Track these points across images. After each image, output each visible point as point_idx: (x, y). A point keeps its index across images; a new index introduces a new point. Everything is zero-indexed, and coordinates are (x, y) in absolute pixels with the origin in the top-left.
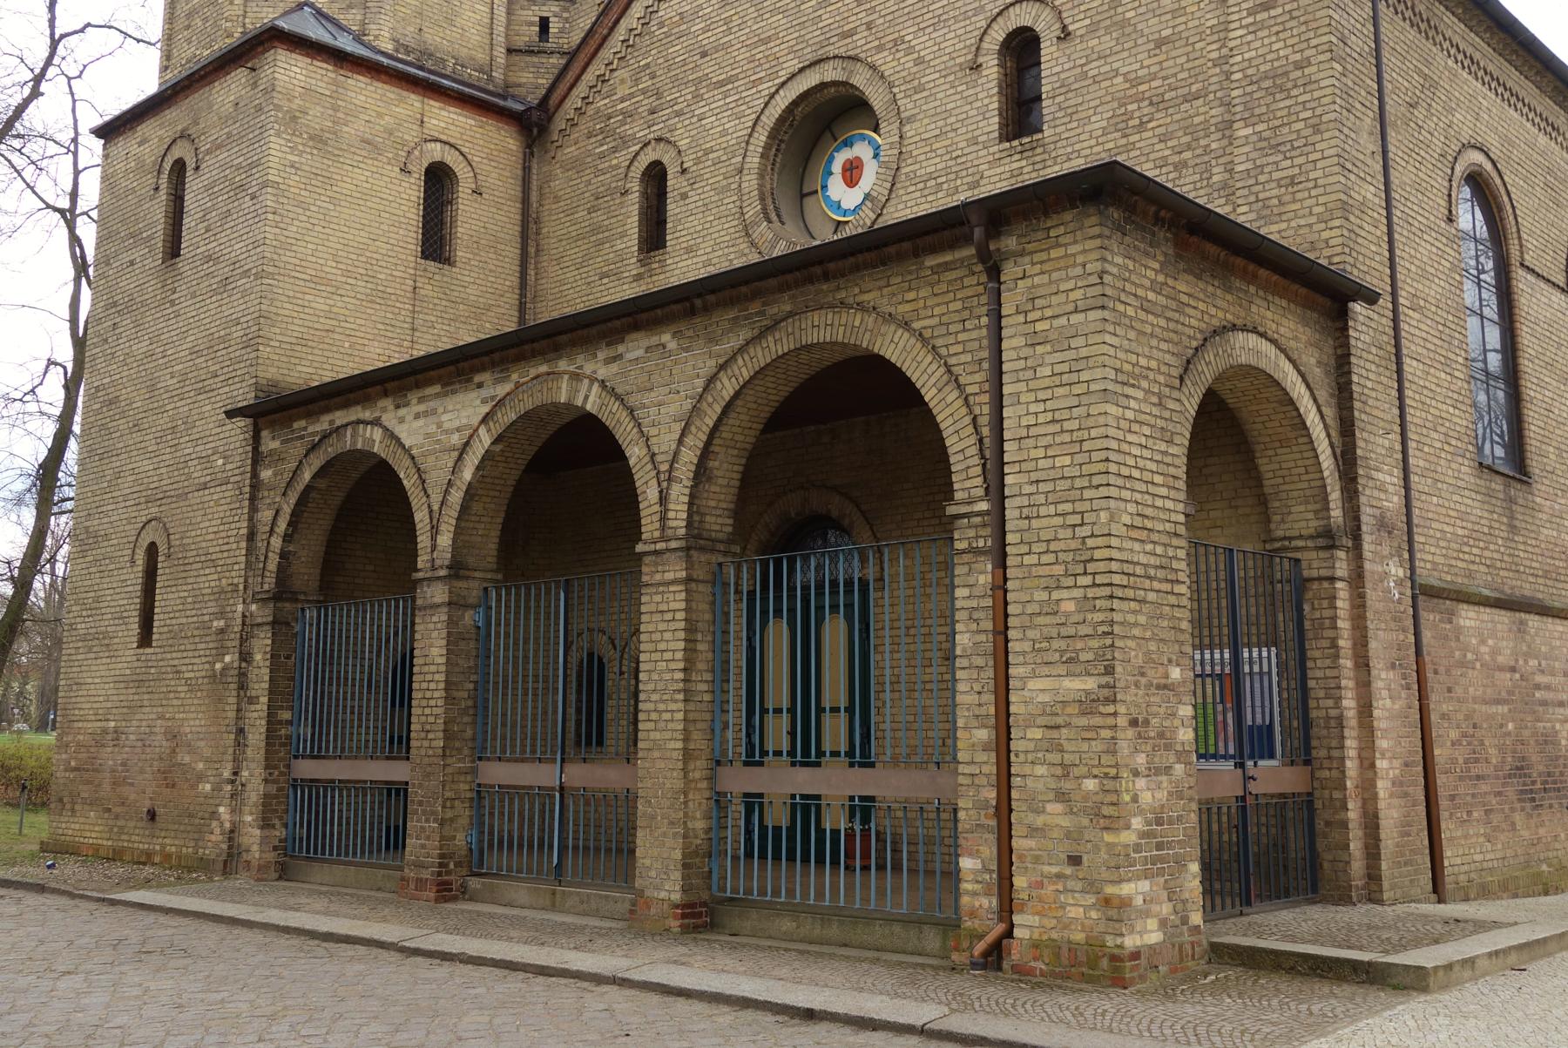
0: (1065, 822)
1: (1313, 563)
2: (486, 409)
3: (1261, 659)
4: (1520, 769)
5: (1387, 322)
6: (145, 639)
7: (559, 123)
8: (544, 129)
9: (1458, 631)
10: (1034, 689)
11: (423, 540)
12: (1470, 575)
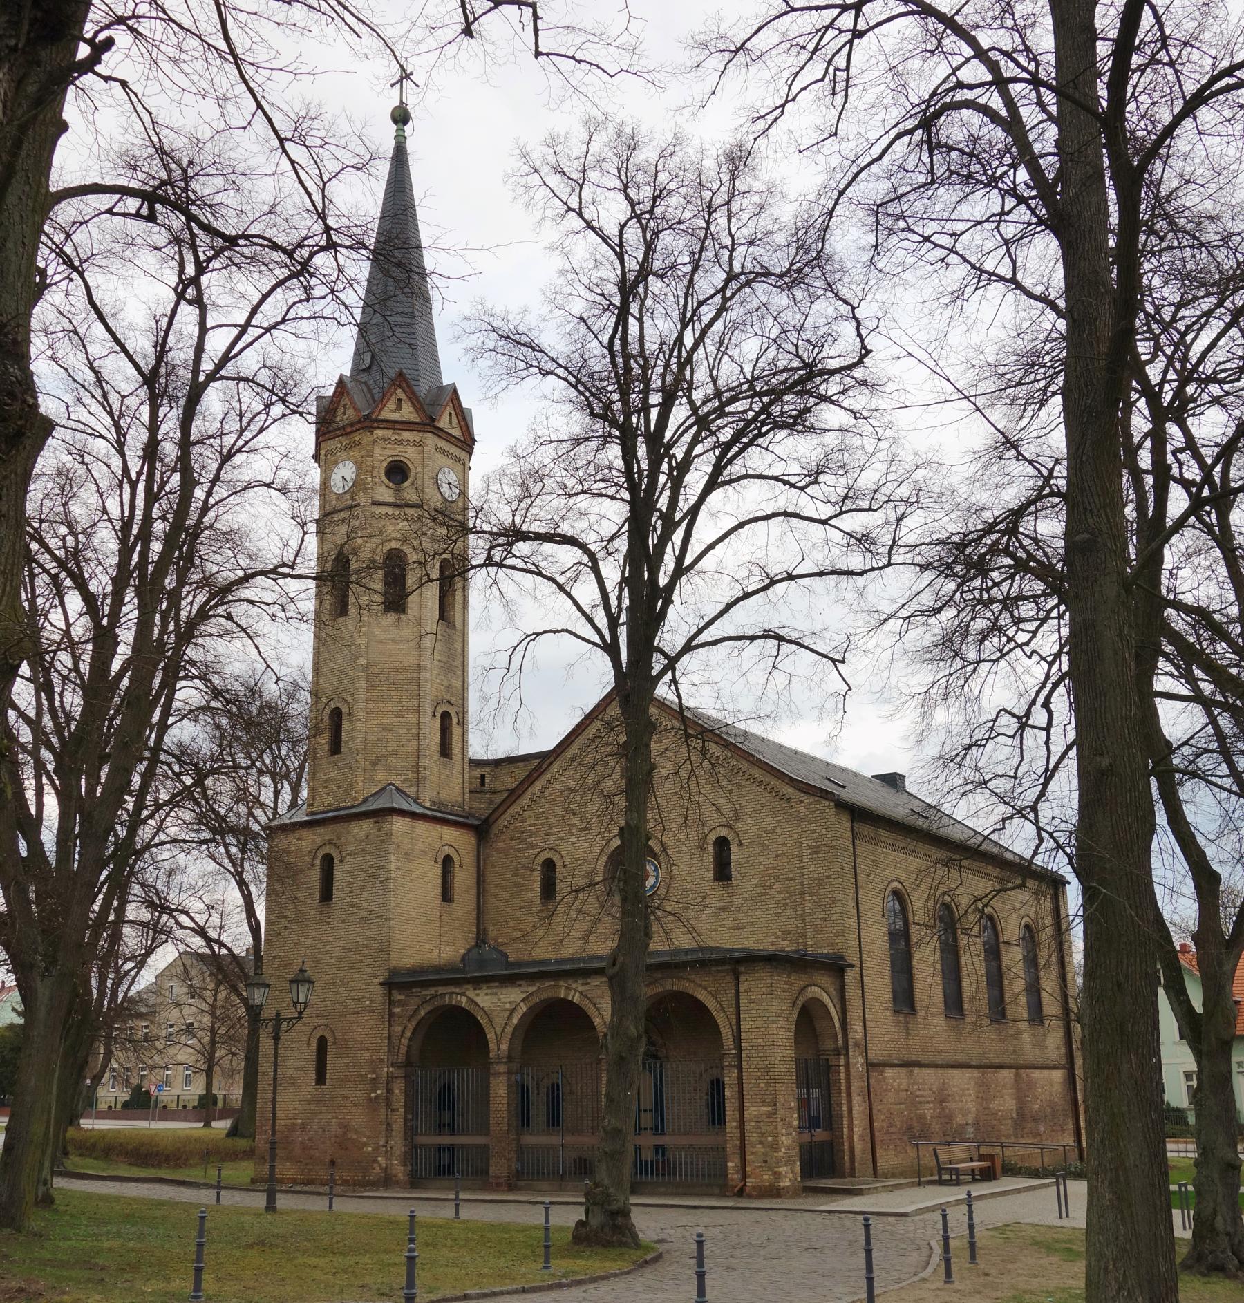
1: (833, 1061)
2: (524, 996)
3: (816, 1092)
4: (909, 1129)
5: (858, 976)
6: (321, 1078)
7: (495, 830)
8: (487, 832)
9: (885, 1078)
10: (752, 1110)
11: (492, 1046)
12: (890, 1055)
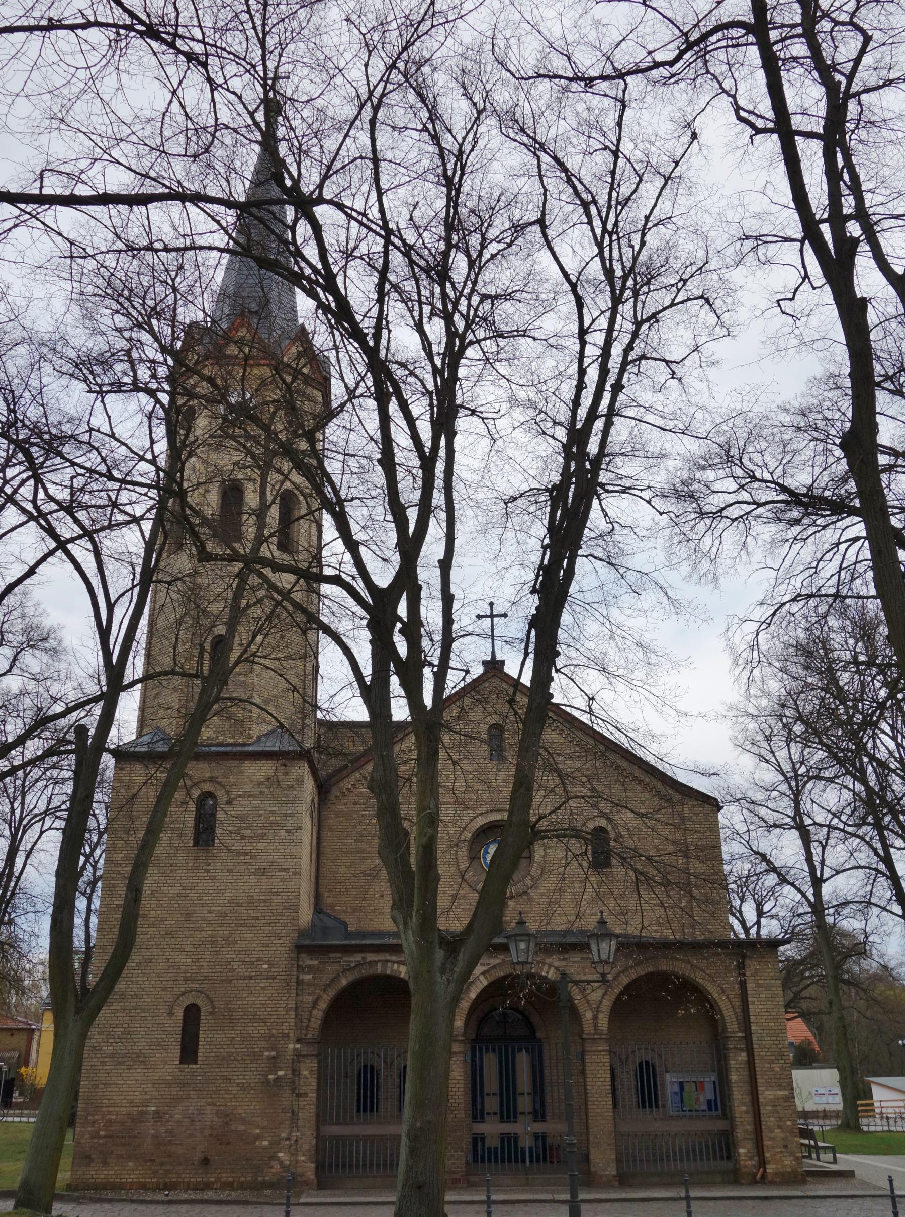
0: (782, 1135)
